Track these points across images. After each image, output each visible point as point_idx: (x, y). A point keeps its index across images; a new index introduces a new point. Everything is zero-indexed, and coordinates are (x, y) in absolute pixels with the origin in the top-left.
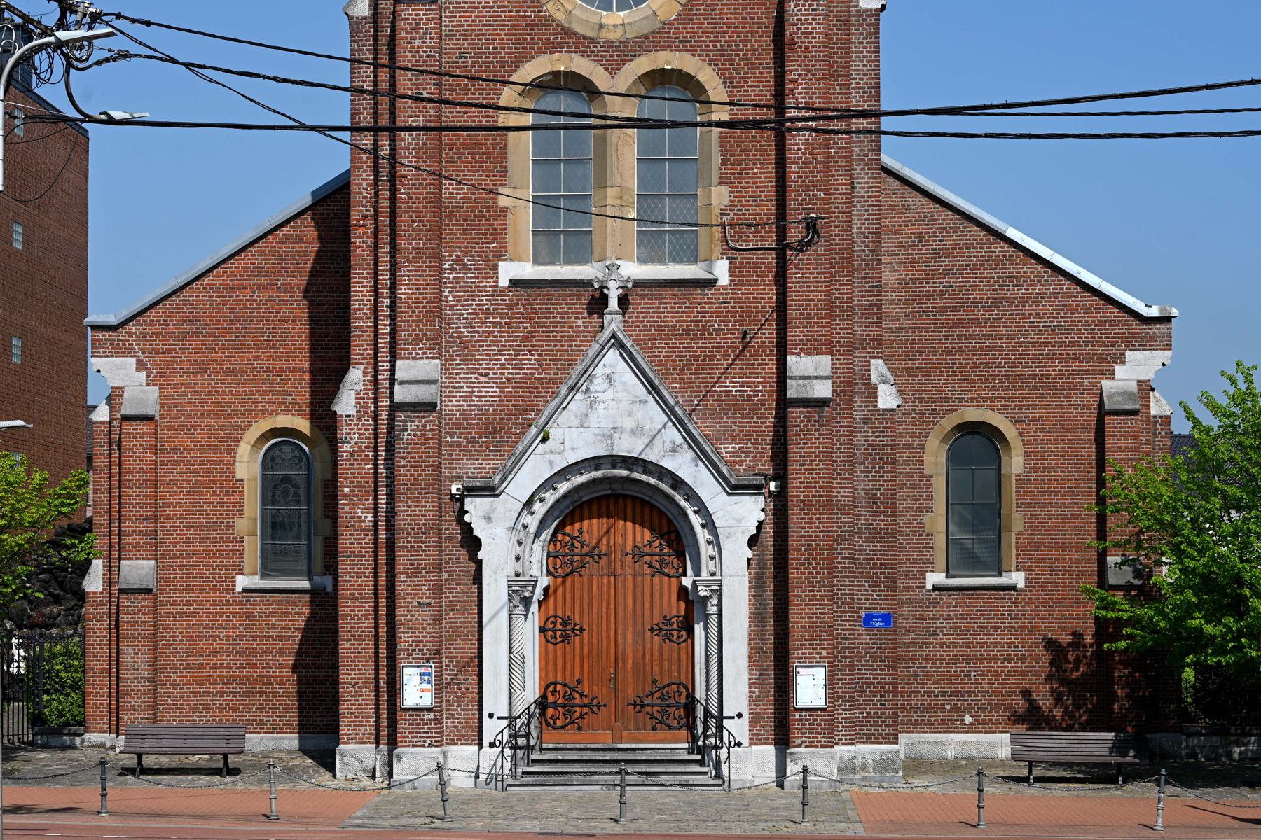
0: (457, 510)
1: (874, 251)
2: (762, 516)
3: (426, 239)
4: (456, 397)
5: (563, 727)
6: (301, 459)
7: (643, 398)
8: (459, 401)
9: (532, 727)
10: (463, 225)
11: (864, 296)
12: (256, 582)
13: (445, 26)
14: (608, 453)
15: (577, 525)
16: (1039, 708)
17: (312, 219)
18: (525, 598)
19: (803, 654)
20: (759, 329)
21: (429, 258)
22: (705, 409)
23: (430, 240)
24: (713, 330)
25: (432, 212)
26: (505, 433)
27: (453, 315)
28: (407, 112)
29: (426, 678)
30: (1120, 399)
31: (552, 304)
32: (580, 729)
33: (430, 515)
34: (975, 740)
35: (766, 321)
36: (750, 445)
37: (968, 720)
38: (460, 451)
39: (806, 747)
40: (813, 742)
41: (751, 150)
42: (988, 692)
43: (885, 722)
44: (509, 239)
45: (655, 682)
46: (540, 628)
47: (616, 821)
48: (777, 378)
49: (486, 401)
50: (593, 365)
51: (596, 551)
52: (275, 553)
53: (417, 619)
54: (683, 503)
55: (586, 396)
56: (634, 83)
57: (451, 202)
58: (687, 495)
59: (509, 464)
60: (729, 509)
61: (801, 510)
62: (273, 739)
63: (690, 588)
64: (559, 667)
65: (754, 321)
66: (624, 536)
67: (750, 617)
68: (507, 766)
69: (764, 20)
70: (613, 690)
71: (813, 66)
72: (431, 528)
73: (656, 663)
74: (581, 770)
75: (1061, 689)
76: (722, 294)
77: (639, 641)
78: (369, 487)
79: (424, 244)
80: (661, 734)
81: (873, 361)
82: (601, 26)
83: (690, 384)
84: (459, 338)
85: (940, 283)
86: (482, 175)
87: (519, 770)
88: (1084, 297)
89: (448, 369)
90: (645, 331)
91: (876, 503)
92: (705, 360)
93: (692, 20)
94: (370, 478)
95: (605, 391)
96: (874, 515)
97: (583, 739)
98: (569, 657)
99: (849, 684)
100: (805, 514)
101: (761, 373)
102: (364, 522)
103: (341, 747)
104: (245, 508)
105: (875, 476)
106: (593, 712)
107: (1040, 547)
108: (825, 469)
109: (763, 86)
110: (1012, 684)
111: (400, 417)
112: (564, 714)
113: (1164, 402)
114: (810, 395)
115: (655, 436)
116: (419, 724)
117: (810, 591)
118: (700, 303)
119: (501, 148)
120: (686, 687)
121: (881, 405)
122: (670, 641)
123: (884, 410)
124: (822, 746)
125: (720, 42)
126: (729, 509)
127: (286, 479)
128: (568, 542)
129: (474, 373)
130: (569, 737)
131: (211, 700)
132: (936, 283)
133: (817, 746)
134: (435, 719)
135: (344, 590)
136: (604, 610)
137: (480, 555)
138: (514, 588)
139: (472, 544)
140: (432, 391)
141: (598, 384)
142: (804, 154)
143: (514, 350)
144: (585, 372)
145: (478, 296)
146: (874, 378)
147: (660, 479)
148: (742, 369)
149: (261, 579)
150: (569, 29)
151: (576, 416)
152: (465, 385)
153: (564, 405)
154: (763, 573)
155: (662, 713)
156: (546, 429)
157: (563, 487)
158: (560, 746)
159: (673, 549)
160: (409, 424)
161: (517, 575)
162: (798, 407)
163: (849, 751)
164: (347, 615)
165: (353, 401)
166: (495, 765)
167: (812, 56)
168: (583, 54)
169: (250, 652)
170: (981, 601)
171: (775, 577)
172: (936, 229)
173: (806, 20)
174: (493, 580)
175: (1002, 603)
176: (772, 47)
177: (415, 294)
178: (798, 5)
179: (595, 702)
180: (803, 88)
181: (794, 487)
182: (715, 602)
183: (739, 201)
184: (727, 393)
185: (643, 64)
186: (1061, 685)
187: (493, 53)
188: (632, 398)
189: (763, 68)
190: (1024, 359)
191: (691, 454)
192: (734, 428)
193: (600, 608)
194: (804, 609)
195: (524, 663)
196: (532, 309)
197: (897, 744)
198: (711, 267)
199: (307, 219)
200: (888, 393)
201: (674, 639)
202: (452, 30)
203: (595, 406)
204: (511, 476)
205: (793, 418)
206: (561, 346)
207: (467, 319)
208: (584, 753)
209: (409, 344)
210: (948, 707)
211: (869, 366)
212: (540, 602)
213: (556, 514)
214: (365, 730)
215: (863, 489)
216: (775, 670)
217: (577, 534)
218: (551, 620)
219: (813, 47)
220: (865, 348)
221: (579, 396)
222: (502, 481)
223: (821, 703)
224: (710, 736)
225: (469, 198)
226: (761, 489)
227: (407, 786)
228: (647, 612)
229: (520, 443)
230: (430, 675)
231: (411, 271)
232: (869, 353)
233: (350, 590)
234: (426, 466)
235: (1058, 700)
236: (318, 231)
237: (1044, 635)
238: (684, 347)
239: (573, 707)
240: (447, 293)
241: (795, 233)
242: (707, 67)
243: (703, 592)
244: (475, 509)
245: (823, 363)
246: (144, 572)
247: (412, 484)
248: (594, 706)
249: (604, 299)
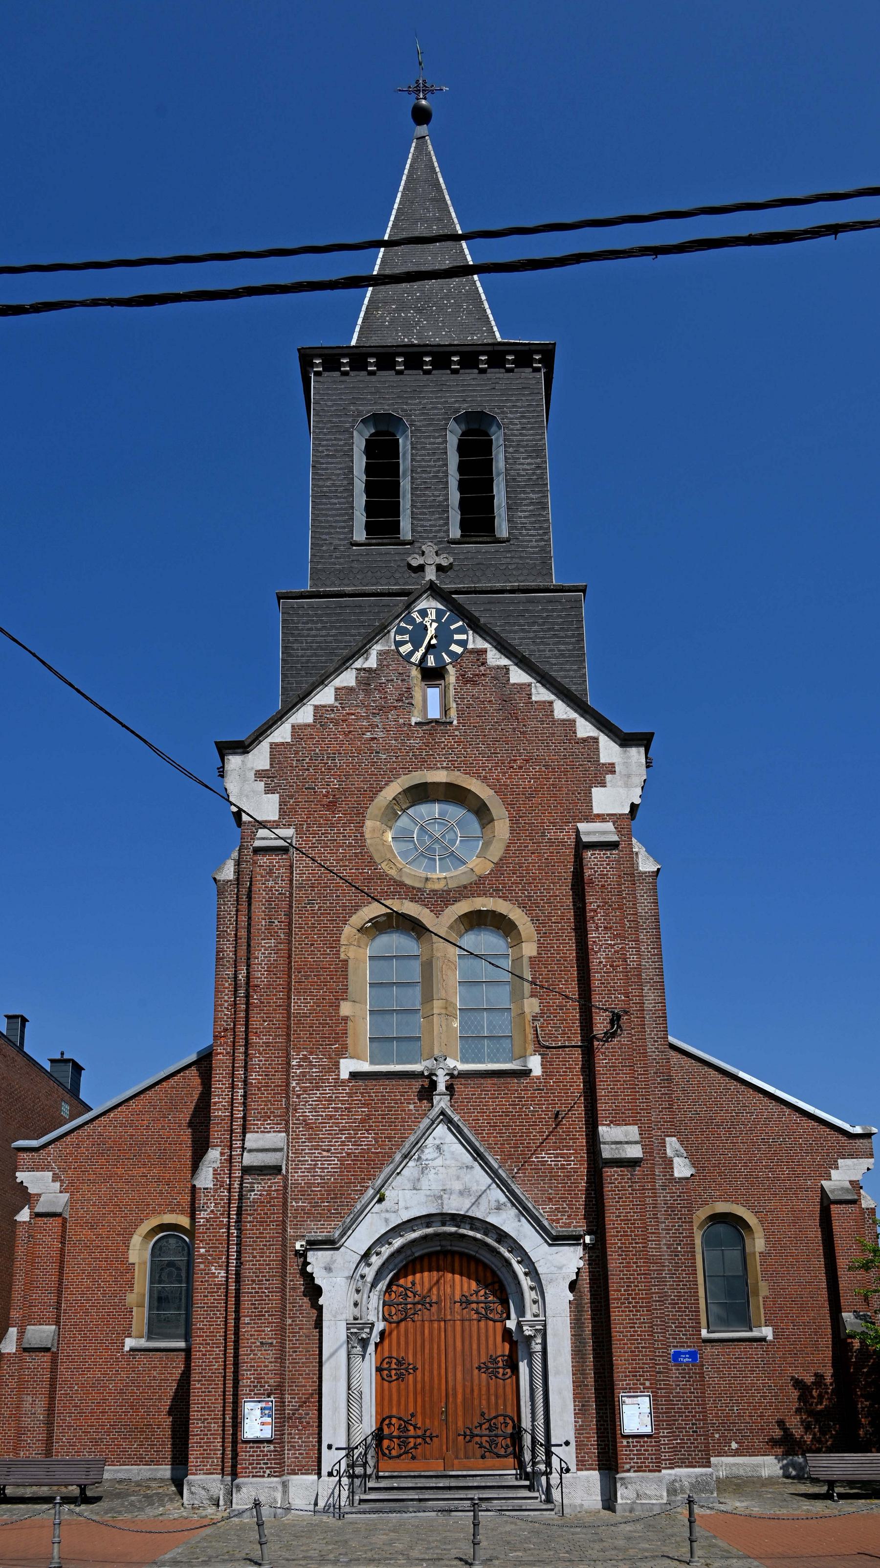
0: (300, 1264)
1: (663, 1052)
2: (581, 1264)
3: (275, 1035)
4: (301, 1169)
5: (399, 1456)
6: (183, 1249)
7: (469, 1164)
8: (304, 1172)
9: (369, 1456)
10: (309, 1031)
11: (656, 1087)
12: (143, 1343)
13: (296, 880)
14: (438, 1211)
15: (410, 1278)
16: (792, 1435)
17: (197, 1070)
18: (363, 1339)
19: (627, 1384)
20: (569, 1111)
21: (277, 1050)
22: (524, 1177)
23: (279, 1035)
24: (529, 1112)
25: (281, 1013)
26: (345, 1198)
27: (300, 1102)
28: (261, 936)
29: (267, 1412)
30: (840, 1192)
31: (386, 1092)
32: (414, 1458)
33: (274, 1264)
34: (741, 1462)
35: (575, 1104)
36: (565, 1206)
37: (734, 1445)
38: (305, 1213)
39: (635, 1471)
40: (641, 1467)
41: (557, 971)
42: (749, 1423)
43: (697, 1447)
44: (349, 1041)
45: (483, 1414)
46: (377, 1368)
47: (467, 1563)
48: (587, 1150)
49: (328, 1172)
50: (424, 1138)
51: (428, 1300)
52: (159, 1321)
53: (259, 1358)
54: (507, 1254)
55: (418, 1163)
56: (456, 921)
57: (300, 1013)
58: (511, 1247)
59: (348, 1220)
60: (550, 1258)
61: (619, 1255)
62: (150, 1470)
63: (514, 1329)
64: (394, 1402)
65: (564, 1104)
66: (453, 1287)
67: (572, 1355)
68: (345, 1494)
69: (563, 874)
70: (444, 1423)
71: (609, 899)
72: (275, 1276)
73: (484, 1397)
74: (417, 1497)
75: (809, 1419)
76: (536, 1083)
77: (468, 1377)
78: (223, 1247)
79: (273, 1039)
80: (489, 1461)
81: (667, 1139)
82: (427, 879)
83: (510, 1156)
84: (304, 1121)
85: (689, 1111)
86: (326, 992)
87: (357, 1498)
88: (802, 1120)
89: (295, 1146)
90: (469, 1113)
91: (678, 1256)
92: (522, 1136)
93: (503, 874)
94: (224, 1240)
95: (435, 1159)
96: (677, 1266)
97: (417, 1467)
98: (403, 1393)
99: (665, 1413)
100: (622, 1259)
101: (573, 1146)
102: (217, 1277)
103: (190, 1477)
104: (135, 1286)
105: (676, 1233)
106: (426, 1442)
107: (783, 1307)
108: (640, 1220)
109: (565, 923)
110: (769, 1416)
111: (249, 1179)
112: (399, 1445)
113: (869, 1198)
114: (623, 1156)
115: (480, 1196)
116: (259, 1456)
117: (631, 1327)
118: (517, 1090)
119: (342, 971)
120: (512, 1420)
121: (677, 1174)
122: (497, 1377)
123: (679, 1179)
124: (650, 1471)
125: (528, 890)
126: (550, 1258)
127: (171, 1264)
128: (402, 1292)
129: (318, 1149)
130: (404, 1465)
131: (99, 1439)
132: (686, 1111)
133: (645, 1471)
134: (275, 1451)
135: (197, 1336)
136: (435, 1351)
137: (321, 1301)
138: (352, 1330)
139: (314, 1291)
140: (277, 1157)
141: (429, 1153)
142: (605, 966)
143: (353, 1130)
144: (417, 1143)
145: (322, 1086)
146: (670, 1153)
147: (486, 1234)
148: (556, 1143)
149: (147, 1341)
150: (400, 882)
151: (409, 1180)
152: (310, 1159)
153: (398, 1171)
154: (581, 1315)
155: (491, 1443)
156: (382, 1191)
157: (398, 1243)
158: (396, 1474)
159: (497, 1298)
160: (256, 1186)
161: (355, 1319)
162: (612, 1167)
163: (670, 1475)
164: (199, 1359)
165: (211, 1176)
166: (333, 1493)
167: (608, 892)
168: (412, 900)
169: (134, 1399)
170: (738, 1350)
171: (592, 1319)
172: (684, 1073)
173: (601, 865)
174: (333, 1322)
175: (756, 1351)
176: (571, 894)
177: (264, 1079)
178: (595, 854)
179: (428, 1434)
180: (601, 916)
181: (612, 1236)
182: (539, 1340)
183: (547, 1010)
184: (544, 1163)
185: (463, 907)
186: (809, 1416)
187: (336, 900)
188: (459, 1164)
189: (564, 909)
190: (759, 1166)
191: (514, 1211)
192: (550, 1191)
193: (431, 1349)
194: (627, 1344)
195: (361, 1398)
196: (369, 1096)
197: (709, 1467)
198: (525, 1062)
199: (193, 1070)
200: (682, 1165)
201: (500, 1376)
202: (302, 884)
203: (426, 1172)
204: (350, 1231)
205: (608, 1176)
206: (395, 1126)
207: (312, 1105)
208: (418, 1480)
209: (257, 1120)
210: (717, 1436)
211: (665, 1143)
212: (377, 1345)
213: (391, 1267)
214: (213, 1462)
215: (665, 1244)
216: (596, 1401)
217: (410, 1286)
218: (387, 1360)
219: (608, 885)
220: (661, 1129)
221: (411, 1164)
222: (342, 1235)
223: (648, 1430)
224: (539, 1463)
225: (314, 1010)
226: (580, 1240)
227: (245, 1515)
228: (475, 1353)
229: (358, 1203)
230: (271, 1409)
231: (261, 1061)
232: (664, 1132)
233: (202, 1336)
234: (271, 1221)
235: (807, 1428)
236: (201, 1079)
237: (792, 1377)
238: (503, 1126)
239: (407, 1438)
240: (294, 1085)
241: (601, 1023)
242: (517, 908)
243: (528, 1332)
244: (317, 1261)
245: (633, 1132)
246: (45, 1335)
247: (257, 1238)
248: (426, 1437)
249: (433, 1085)
